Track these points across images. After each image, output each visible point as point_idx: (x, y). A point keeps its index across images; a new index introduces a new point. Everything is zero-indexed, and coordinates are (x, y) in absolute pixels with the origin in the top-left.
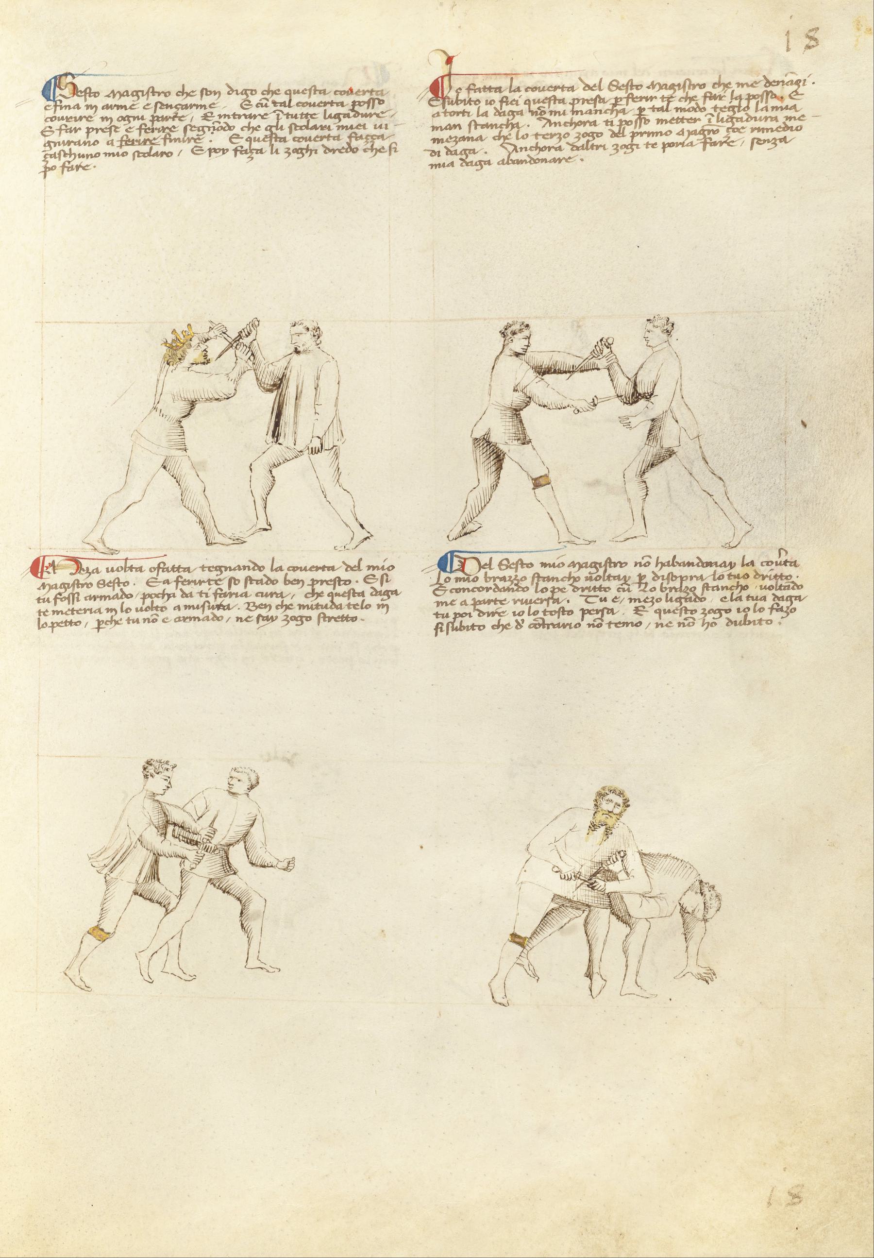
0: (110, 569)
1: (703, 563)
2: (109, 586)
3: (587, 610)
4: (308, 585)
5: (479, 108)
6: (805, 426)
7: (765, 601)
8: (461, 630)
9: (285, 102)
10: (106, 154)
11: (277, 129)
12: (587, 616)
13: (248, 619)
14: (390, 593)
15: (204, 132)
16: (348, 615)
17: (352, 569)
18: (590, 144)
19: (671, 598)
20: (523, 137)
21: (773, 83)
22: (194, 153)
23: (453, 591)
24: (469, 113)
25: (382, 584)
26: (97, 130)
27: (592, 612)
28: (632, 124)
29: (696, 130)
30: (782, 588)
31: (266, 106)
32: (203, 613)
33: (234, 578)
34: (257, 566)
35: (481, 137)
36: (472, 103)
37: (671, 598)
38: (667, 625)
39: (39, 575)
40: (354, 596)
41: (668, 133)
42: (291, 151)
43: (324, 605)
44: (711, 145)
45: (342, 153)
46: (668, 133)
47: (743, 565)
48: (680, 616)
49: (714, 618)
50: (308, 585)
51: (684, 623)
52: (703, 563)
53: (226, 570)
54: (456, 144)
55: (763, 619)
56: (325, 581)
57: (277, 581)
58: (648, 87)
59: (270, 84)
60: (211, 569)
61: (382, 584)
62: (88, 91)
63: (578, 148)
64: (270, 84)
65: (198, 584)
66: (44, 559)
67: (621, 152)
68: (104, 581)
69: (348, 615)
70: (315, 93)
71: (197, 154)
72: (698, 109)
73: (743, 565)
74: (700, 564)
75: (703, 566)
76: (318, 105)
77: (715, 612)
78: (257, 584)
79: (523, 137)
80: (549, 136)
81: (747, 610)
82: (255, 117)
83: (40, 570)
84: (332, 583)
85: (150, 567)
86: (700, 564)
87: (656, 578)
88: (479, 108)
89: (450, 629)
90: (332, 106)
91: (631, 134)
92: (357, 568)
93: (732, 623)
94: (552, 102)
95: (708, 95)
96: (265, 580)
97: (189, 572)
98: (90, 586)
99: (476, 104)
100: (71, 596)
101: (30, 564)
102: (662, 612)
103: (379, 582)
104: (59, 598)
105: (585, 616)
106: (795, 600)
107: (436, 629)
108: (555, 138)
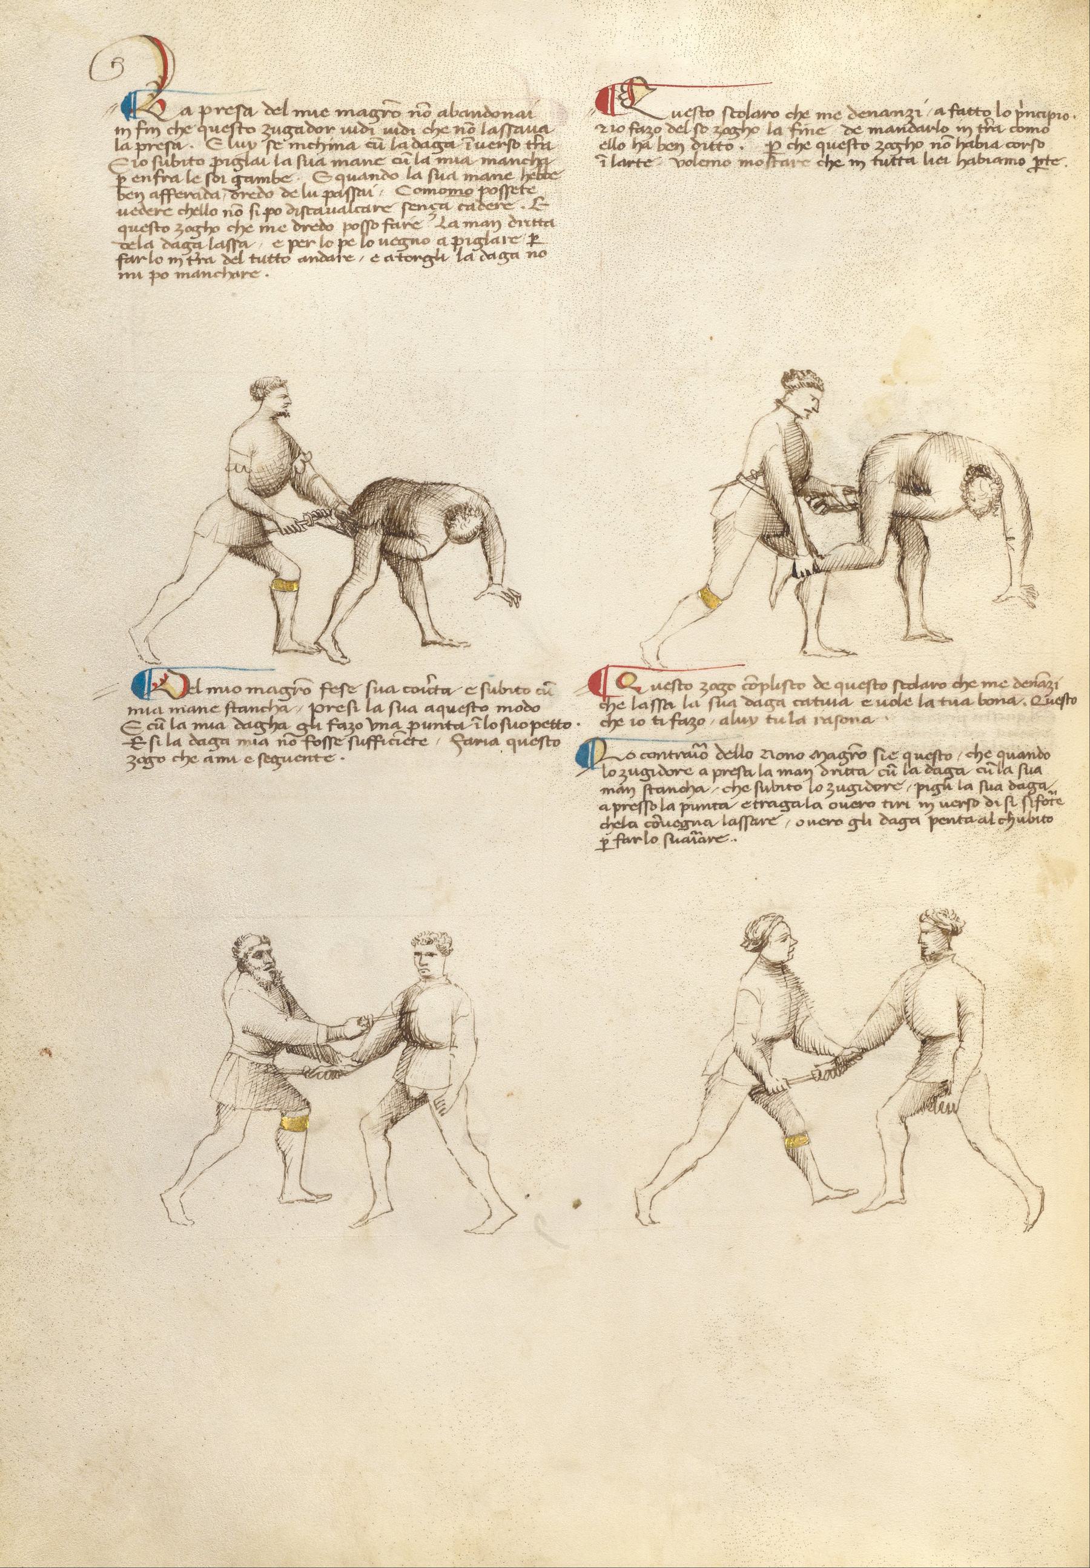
2: (460, 712)
4: (687, 782)
7: (972, 789)
9: (445, 111)
10: (466, 223)
12: (296, 249)
16: (559, 720)
17: (676, 131)
19: (932, 160)
27: (334, 690)
30: (561, 726)
32: (1032, 152)
33: (307, 207)
37: (932, 160)
38: (279, 230)
39: (609, 112)
40: (875, 688)
48: (467, 715)
50: (687, 782)
51: (839, 771)
59: (797, 106)
62: (154, 225)
68: (275, 688)
69: (559, 720)
70: (548, 745)
78: (769, 806)
83: (610, 94)
84: (846, 146)
90: (638, 166)
95: (621, 837)
96: (359, 128)
100: (365, 224)
105: (934, 826)
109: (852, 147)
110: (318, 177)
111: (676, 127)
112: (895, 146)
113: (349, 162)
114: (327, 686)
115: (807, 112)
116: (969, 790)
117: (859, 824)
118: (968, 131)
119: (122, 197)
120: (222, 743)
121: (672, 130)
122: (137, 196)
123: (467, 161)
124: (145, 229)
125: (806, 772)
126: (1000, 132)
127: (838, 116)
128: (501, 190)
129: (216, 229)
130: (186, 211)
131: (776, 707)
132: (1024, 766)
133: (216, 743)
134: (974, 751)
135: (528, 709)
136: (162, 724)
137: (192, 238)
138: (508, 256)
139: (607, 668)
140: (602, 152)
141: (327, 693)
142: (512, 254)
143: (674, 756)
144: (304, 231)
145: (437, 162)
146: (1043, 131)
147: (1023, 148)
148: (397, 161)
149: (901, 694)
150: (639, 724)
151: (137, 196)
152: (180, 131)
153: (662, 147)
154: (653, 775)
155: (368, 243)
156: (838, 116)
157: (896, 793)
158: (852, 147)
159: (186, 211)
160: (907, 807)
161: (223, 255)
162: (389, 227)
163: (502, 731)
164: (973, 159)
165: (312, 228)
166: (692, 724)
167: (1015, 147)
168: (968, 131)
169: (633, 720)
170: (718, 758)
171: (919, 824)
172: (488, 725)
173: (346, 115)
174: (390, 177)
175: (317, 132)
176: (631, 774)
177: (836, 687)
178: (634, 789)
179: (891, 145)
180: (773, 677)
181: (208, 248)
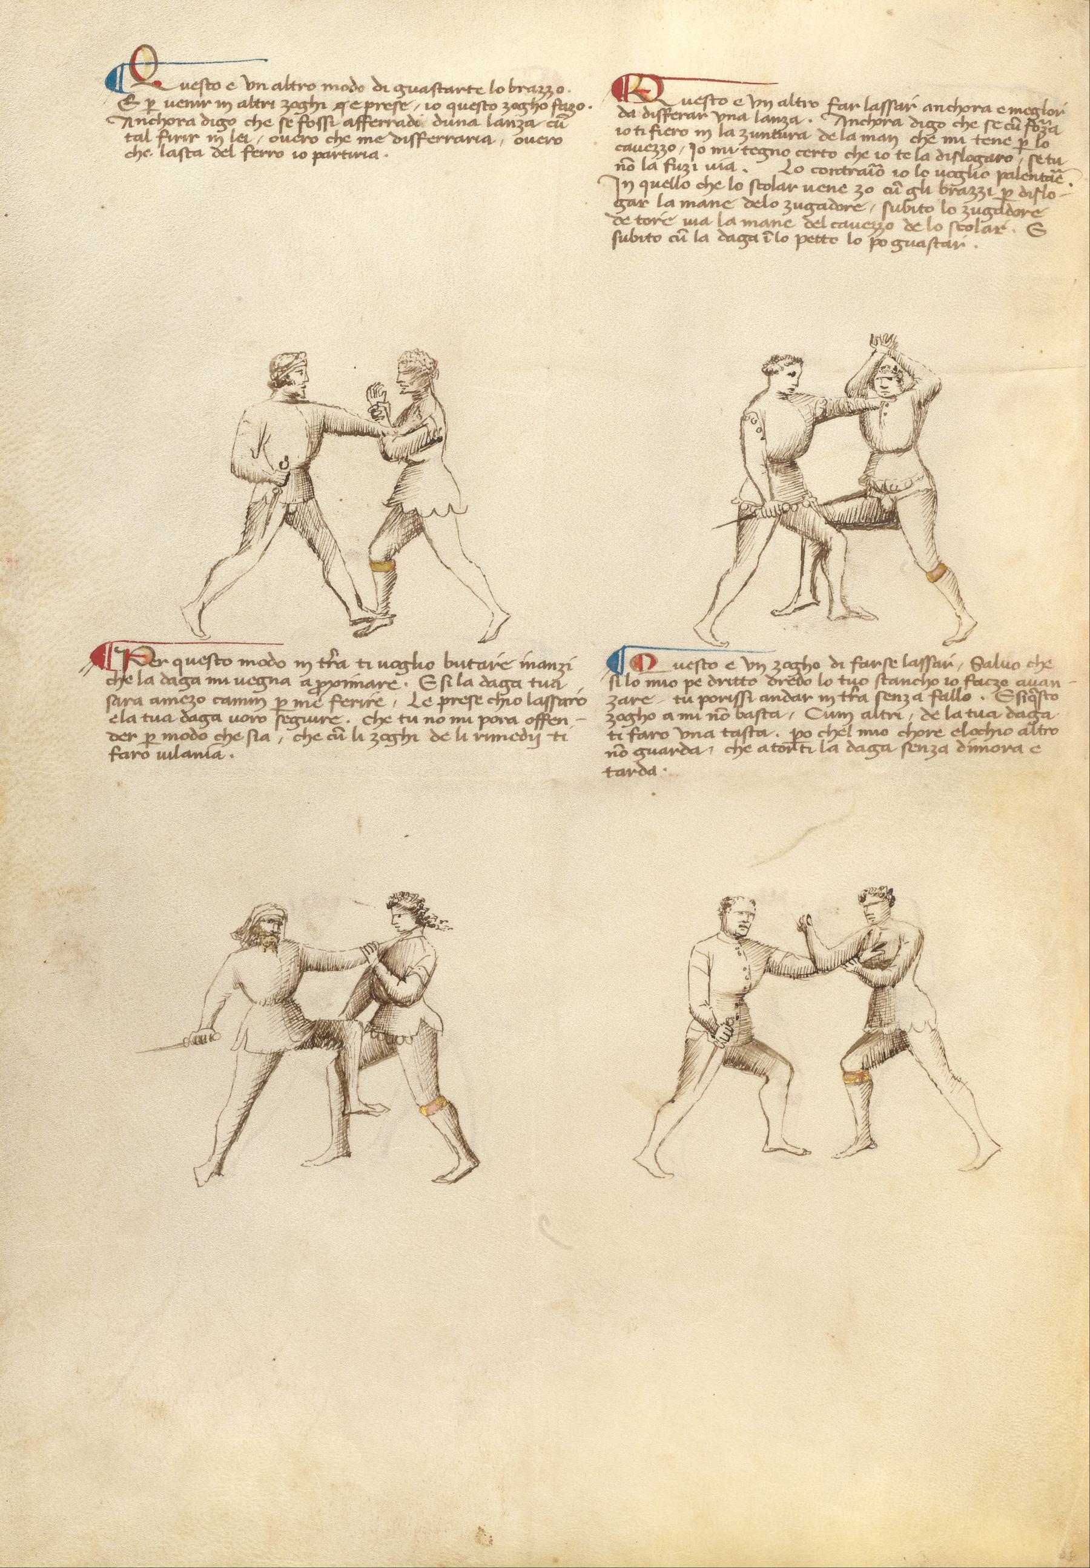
1: (837, 206)
3: (487, 717)
8: (632, 241)
9: (785, 101)
13: (727, 205)
14: (510, 684)
21: (123, 737)
23: (668, 132)
24: (368, 663)
25: (1018, 703)
27: (345, 703)
28: (699, 149)
31: (684, 240)
36: (487, 108)
41: (673, 684)
44: (861, 667)
45: (432, 143)
46: (673, 684)
47: (721, 135)
52: (837, 206)
54: (288, 110)
55: (728, 730)
57: (231, 661)
58: (796, 186)
59: (416, 653)
60: (754, 151)
61: (1018, 703)
63: (754, 205)
64: (416, 653)
65: (494, 663)
66: (623, 652)
67: (382, 744)
71: (1035, 236)
73: (721, 135)
74: (834, 207)
75: (837, 209)
76: (864, 227)
80: (184, 104)
83: (118, 74)
85: (362, 718)
86: (834, 207)
89: (252, 738)
92: (820, 225)
97: (778, 717)
98: (684, 133)
101: (92, 651)
102: (457, 108)
103: (1015, 701)
104: (116, 754)
107: (614, 239)
109: (437, 91)
110: (810, 713)
111: (856, 746)
112: (628, 718)
113: (1003, 731)
114: (835, 101)
116: (469, 687)
117: (918, 192)
119: (740, 715)
120: (818, 208)
121: (824, 138)
125: (845, 715)
127: (1007, 142)
128: (319, 123)
129: (935, 682)
130: (854, 155)
134: (985, 728)
136: (897, 189)
137: (218, 131)
139: (624, 647)
141: (337, 705)
143: (886, 716)
146: (840, 190)
147: (655, 223)
150: (301, 156)
152: (958, 110)
153: (449, 664)
156: (1007, 142)
157: (936, 722)
158: (437, 91)
159: (955, 107)
160: (899, 718)
162: (937, 699)
165: (460, 700)
166: (973, 193)
167: (646, 224)
169: (166, 102)
172: (630, 682)
177: (174, 663)
179: (516, 106)
180: (806, 657)
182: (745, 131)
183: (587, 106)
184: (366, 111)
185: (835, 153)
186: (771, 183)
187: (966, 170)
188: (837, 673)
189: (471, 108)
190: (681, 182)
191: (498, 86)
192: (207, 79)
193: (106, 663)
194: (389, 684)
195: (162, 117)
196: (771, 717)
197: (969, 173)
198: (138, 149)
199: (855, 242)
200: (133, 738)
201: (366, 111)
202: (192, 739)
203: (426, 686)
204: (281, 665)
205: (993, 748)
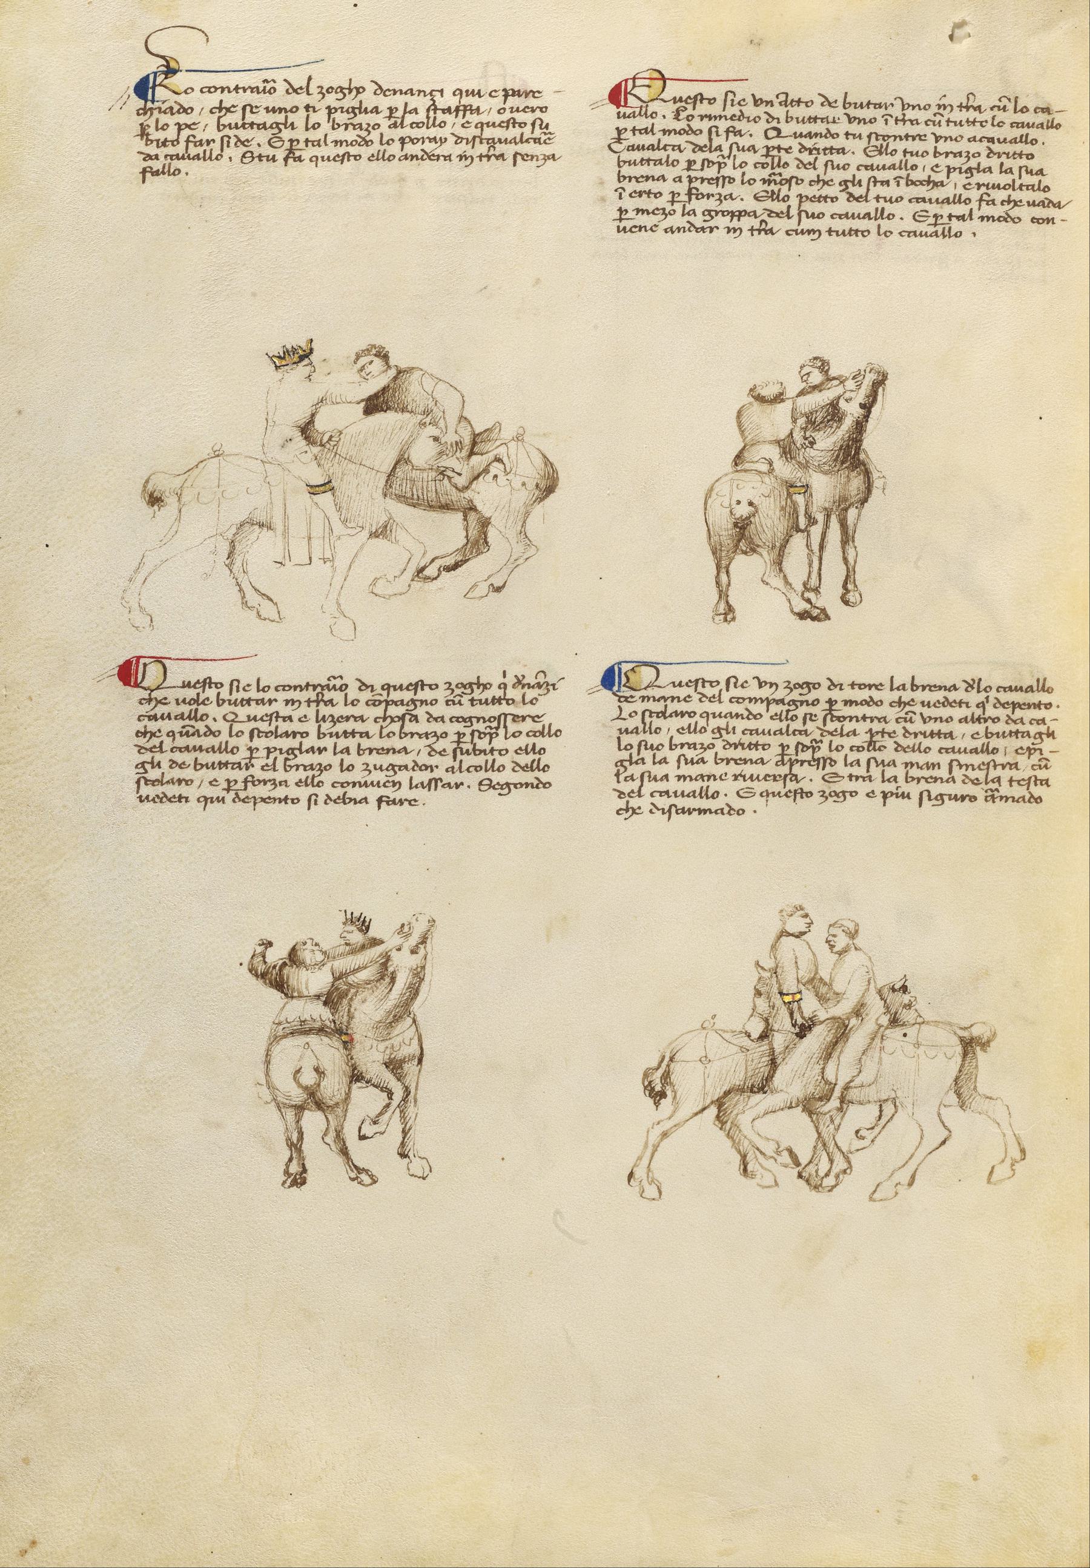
0: (326, 158)
5: (346, 695)
6: (504, 672)
11: (728, 733)
15: (1042, 740)
18: (791, 714)
20: (313, 127)
22: (916, 220)
26: (946, 139)
29: (975, 137)
31: (460, 703)
34: (184, 108)
35: (405, 748)
42: (324, 91)
43: (398, 685)
49: (801, 694)
53: (801, 705)
56: (874, 685)
71: (920, 221)
72: (871, 703)
77: (801, 686)
79: (313, 127)
81: (988, 689)
82: (524, 718)
87: (832, 687)
88: (346, 695)
89: (643, 748)
90: (649, 197)
91: (503, 93)
93: (731, 746)
94: (798, 796)
98: (370, 143)
99: (217, 687)
101: (600, 678)
106: (400, 770)
108: (269, 786)
113: (810, 702)
115: (444, 750)
118: (817, 233)
122: (394, 785)
123: (1015, 766)
124: (265, 718)
126: (333, 706)
131: (398, 772)
132: (643, 743)
133: (393, 769)
135: (851, 199)
136: (911, 718)
138: (396, 769)
140: (621, 185)
142: (400, 767)
144: (727, 764)
145: (635, 212)
148: (517, 734)
149: (461, 761)
151: (394, 785)
153: (910, 183)
154: (360, 113)
155: (749, 181)
161: (1007, 716)
163: (973, 714)
164: (694, 792)
168: (817, 233)
170: (513, 770)
171: (668, 781)
173: (850, 721)
174: (1013, 220)
175: (840, 721)
176: (375, 769)
178: (777, 686)
181: (378, 735)
182: (368, 765)
183: (466, 785)
184: (791, 769)
185: (856, 793)
186: (160, 778)
187: (297, 746)
188: (366, 695)
189: (407, 689)
190: (316, 781)
191: (985, 685)
192: (701, 94)
193: (133, 680)
194: (931, 687)
195: (223, 106)
196: (313, 145)
197: (152, 763)
198: (903, 700)
199: (925, 752)
200: (274, 702)
201: (791, 769)
202: (869, 706)
203: (869, 154)
204: (1016, 220)
205: (813, 701)
